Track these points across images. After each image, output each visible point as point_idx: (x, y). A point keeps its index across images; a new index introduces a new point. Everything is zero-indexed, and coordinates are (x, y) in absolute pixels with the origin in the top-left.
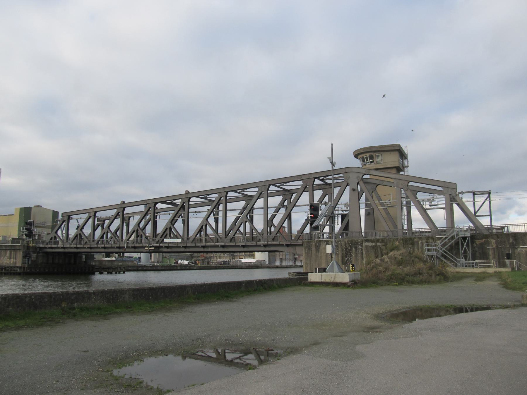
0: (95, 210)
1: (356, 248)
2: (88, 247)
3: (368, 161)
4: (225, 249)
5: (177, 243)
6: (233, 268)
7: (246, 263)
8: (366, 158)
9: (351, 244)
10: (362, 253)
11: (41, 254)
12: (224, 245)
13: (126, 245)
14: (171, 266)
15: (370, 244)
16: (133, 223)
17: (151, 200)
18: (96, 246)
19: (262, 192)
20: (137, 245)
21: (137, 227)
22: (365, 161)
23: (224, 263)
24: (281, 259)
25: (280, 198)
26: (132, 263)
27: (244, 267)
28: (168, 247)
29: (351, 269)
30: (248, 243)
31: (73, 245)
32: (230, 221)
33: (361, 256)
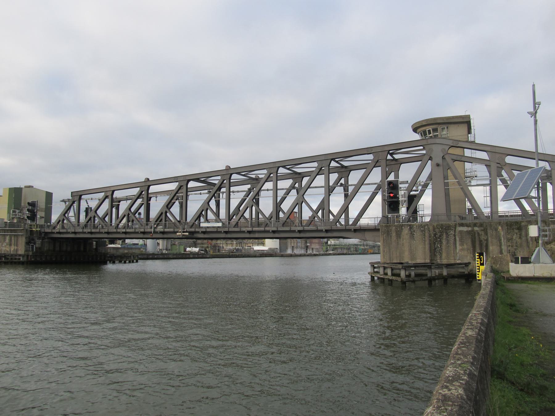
0: (113, 189)
1: (447, 234)
2: (105, 233)
3: (431, 135)
4: (252, 235)
5: (219, 227)
6: (247, 256)
7: (258, 251)
8: (429, 131)
9: (442, 228)
10: (455, 239)
13: (152, 230)
14: (180, 254)
15: (465, 229)
16: (124, 206)
17: (182, 177)
18: (116, 231)
19: (322, 168)
20: (128, 230)
21: (63, 217)
22: (427, 135)
24: (293, 247)
27: (257, 256)
28: (204, 233)
29: (477, 258)
30: (255, 229)
31: (57, 230)
32: (234, 204)
33: (454, 243)
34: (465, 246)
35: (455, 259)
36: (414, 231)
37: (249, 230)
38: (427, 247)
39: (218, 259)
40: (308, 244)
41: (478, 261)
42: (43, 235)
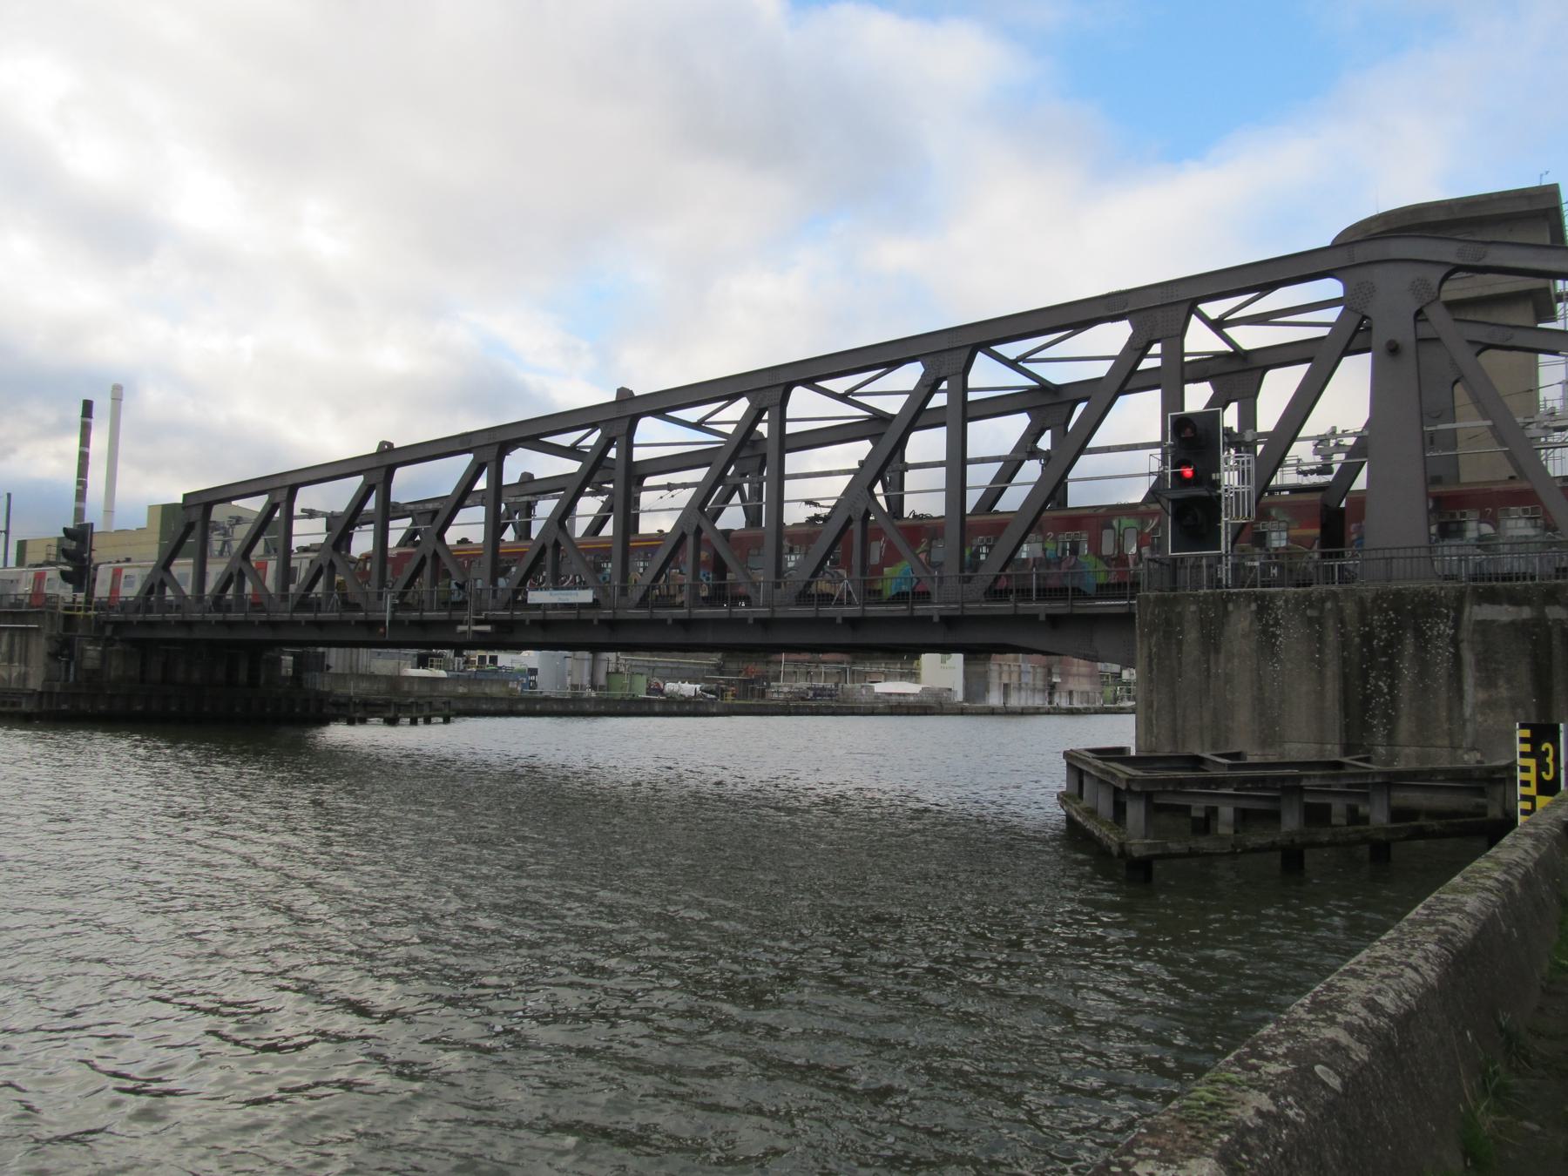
0: (290, 481)
1: (1419, 634)
9: (1396, 611)
10: (1457, 659)
11: (118, 647)
12: (768, 615)
14: (636, 701)
15: (1503, 613)
23: (815, 695)
24: (1006, 686)
25: (1015, 426)
26: (504, 689)
29: (1523, 755)
33: (1450, 676)
34: (1503, 691)
35: (1454, 747)
36: (1277, 623)
37: (680, 617)
38: (1332, 689)
39: (531, 719)
40: (1056, 679)
41: (1525, 769)
42: (108, 631)
